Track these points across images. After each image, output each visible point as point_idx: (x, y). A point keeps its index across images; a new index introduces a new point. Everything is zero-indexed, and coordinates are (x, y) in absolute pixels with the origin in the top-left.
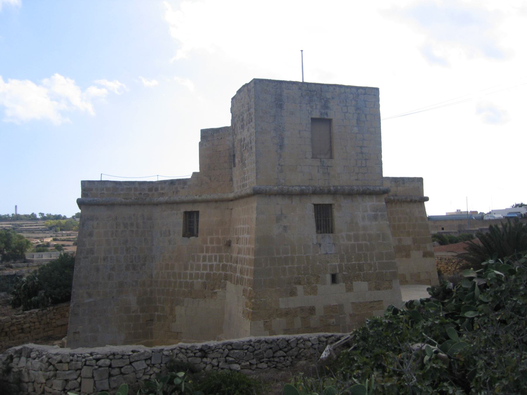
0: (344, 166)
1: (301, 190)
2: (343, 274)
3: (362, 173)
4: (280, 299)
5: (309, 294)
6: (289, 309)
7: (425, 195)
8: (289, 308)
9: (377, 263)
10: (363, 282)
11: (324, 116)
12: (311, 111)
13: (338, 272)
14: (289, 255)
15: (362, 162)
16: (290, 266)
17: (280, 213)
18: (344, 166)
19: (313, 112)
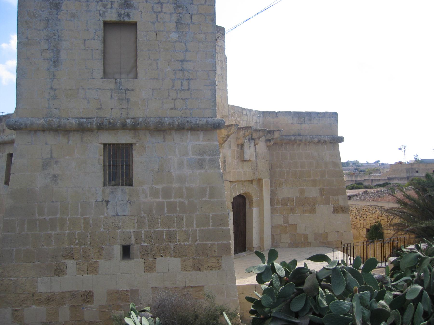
0: (153, 90)
1: (78, 123)
2: (142, 246)
3: (182, 99)
4: (39, 278)
5: (85, 273)
6: (53, 294)
7: (340, 134)
8: (52, 292)
9: (198, 231)
10: (173, 258)
11: (123, 18)
12: (104, 12)
13: (133, 242)
14: (58, 216)
15: (182, 83)
16: (58, 231)
17: (50, 157)
18: (153, 90)
19: (106, 13)
